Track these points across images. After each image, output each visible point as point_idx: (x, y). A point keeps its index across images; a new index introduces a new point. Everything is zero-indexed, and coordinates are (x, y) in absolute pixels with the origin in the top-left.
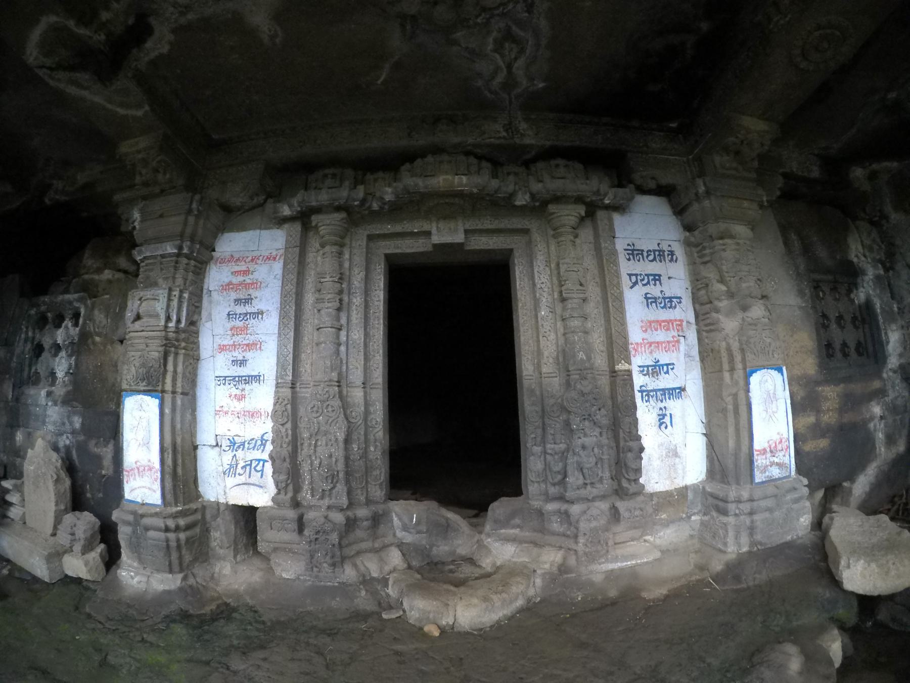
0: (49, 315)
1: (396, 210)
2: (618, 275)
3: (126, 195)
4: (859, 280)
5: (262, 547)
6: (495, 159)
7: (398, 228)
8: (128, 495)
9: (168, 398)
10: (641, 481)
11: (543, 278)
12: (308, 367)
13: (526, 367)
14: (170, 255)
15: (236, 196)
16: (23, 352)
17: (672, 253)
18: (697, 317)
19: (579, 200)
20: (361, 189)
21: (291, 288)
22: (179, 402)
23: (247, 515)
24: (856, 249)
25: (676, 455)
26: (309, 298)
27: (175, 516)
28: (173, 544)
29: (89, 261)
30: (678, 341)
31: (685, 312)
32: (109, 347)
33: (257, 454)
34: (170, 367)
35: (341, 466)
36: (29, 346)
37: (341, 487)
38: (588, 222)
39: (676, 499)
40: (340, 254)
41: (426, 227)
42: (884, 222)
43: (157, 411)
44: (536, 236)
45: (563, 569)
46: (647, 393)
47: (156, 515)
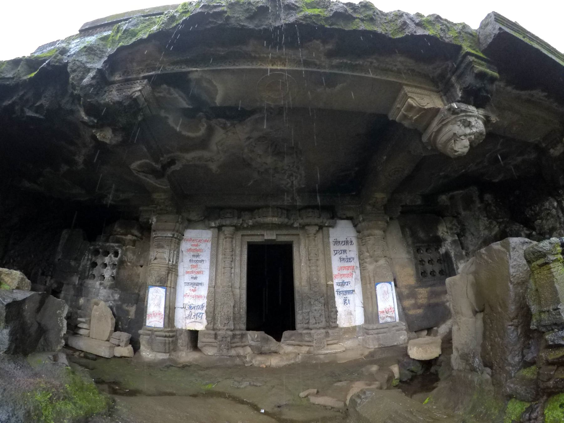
0: (100, 250)
1: (253, 227)
2: (330, 250)
3: (145, 208)
4: (443, 244)
5: (199, 345)
6: (289, 210)
7: (253, 233)
8: (147, 324)
9: (168, 289)
10: (338, 323)
11: (303, 252)
12: (219, 281)
13: (297, 283)
14: (169, 237)
15: (193, 216)
16: (86, 265)
17: (351, 242)
18: (360, 264)
19: (316, 225)
20: (241, 220)
21: (214, 253)
22: (172, 291)
23: (194, 334)
24: (442, 231)
25: (351, 314)
26: (220, 257)
27: (168, 332)
28: (167, 342)
29: (117, 228)
30: (352, 274)
31: (356, 263)
32: (135, 268)
33: (200, 311)
34: (169, 278)
35: (232, 315)
36: (89, 263)
37: (231, 322)
38: (321, 231)
39: (352, 330)
40: (232, 241)
41: (262, 233)
42: (459, 216)
43: (164, 293)
44: (301, 237)
45: (309, 352)
46: (339, 292)
47: (161, 331)
